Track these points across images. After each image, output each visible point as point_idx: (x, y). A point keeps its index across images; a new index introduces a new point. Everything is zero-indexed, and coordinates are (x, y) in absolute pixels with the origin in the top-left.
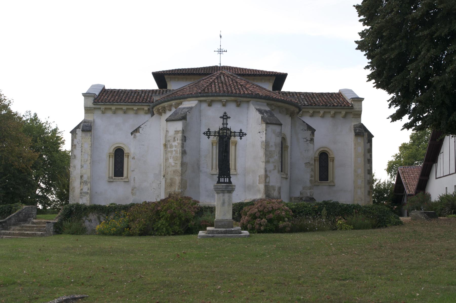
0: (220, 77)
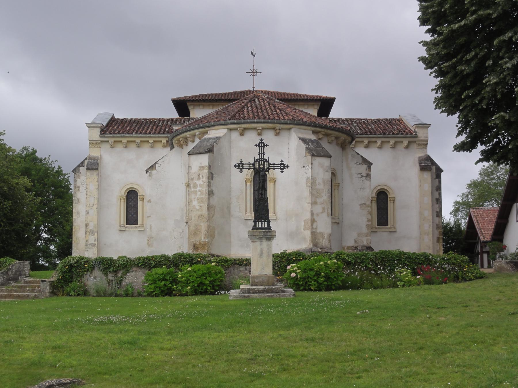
0: (254, 100)
